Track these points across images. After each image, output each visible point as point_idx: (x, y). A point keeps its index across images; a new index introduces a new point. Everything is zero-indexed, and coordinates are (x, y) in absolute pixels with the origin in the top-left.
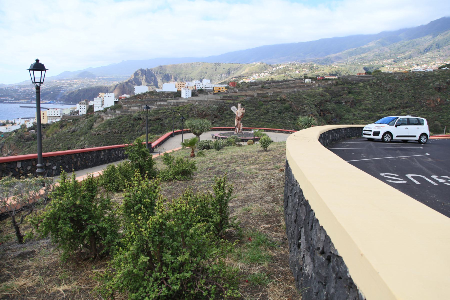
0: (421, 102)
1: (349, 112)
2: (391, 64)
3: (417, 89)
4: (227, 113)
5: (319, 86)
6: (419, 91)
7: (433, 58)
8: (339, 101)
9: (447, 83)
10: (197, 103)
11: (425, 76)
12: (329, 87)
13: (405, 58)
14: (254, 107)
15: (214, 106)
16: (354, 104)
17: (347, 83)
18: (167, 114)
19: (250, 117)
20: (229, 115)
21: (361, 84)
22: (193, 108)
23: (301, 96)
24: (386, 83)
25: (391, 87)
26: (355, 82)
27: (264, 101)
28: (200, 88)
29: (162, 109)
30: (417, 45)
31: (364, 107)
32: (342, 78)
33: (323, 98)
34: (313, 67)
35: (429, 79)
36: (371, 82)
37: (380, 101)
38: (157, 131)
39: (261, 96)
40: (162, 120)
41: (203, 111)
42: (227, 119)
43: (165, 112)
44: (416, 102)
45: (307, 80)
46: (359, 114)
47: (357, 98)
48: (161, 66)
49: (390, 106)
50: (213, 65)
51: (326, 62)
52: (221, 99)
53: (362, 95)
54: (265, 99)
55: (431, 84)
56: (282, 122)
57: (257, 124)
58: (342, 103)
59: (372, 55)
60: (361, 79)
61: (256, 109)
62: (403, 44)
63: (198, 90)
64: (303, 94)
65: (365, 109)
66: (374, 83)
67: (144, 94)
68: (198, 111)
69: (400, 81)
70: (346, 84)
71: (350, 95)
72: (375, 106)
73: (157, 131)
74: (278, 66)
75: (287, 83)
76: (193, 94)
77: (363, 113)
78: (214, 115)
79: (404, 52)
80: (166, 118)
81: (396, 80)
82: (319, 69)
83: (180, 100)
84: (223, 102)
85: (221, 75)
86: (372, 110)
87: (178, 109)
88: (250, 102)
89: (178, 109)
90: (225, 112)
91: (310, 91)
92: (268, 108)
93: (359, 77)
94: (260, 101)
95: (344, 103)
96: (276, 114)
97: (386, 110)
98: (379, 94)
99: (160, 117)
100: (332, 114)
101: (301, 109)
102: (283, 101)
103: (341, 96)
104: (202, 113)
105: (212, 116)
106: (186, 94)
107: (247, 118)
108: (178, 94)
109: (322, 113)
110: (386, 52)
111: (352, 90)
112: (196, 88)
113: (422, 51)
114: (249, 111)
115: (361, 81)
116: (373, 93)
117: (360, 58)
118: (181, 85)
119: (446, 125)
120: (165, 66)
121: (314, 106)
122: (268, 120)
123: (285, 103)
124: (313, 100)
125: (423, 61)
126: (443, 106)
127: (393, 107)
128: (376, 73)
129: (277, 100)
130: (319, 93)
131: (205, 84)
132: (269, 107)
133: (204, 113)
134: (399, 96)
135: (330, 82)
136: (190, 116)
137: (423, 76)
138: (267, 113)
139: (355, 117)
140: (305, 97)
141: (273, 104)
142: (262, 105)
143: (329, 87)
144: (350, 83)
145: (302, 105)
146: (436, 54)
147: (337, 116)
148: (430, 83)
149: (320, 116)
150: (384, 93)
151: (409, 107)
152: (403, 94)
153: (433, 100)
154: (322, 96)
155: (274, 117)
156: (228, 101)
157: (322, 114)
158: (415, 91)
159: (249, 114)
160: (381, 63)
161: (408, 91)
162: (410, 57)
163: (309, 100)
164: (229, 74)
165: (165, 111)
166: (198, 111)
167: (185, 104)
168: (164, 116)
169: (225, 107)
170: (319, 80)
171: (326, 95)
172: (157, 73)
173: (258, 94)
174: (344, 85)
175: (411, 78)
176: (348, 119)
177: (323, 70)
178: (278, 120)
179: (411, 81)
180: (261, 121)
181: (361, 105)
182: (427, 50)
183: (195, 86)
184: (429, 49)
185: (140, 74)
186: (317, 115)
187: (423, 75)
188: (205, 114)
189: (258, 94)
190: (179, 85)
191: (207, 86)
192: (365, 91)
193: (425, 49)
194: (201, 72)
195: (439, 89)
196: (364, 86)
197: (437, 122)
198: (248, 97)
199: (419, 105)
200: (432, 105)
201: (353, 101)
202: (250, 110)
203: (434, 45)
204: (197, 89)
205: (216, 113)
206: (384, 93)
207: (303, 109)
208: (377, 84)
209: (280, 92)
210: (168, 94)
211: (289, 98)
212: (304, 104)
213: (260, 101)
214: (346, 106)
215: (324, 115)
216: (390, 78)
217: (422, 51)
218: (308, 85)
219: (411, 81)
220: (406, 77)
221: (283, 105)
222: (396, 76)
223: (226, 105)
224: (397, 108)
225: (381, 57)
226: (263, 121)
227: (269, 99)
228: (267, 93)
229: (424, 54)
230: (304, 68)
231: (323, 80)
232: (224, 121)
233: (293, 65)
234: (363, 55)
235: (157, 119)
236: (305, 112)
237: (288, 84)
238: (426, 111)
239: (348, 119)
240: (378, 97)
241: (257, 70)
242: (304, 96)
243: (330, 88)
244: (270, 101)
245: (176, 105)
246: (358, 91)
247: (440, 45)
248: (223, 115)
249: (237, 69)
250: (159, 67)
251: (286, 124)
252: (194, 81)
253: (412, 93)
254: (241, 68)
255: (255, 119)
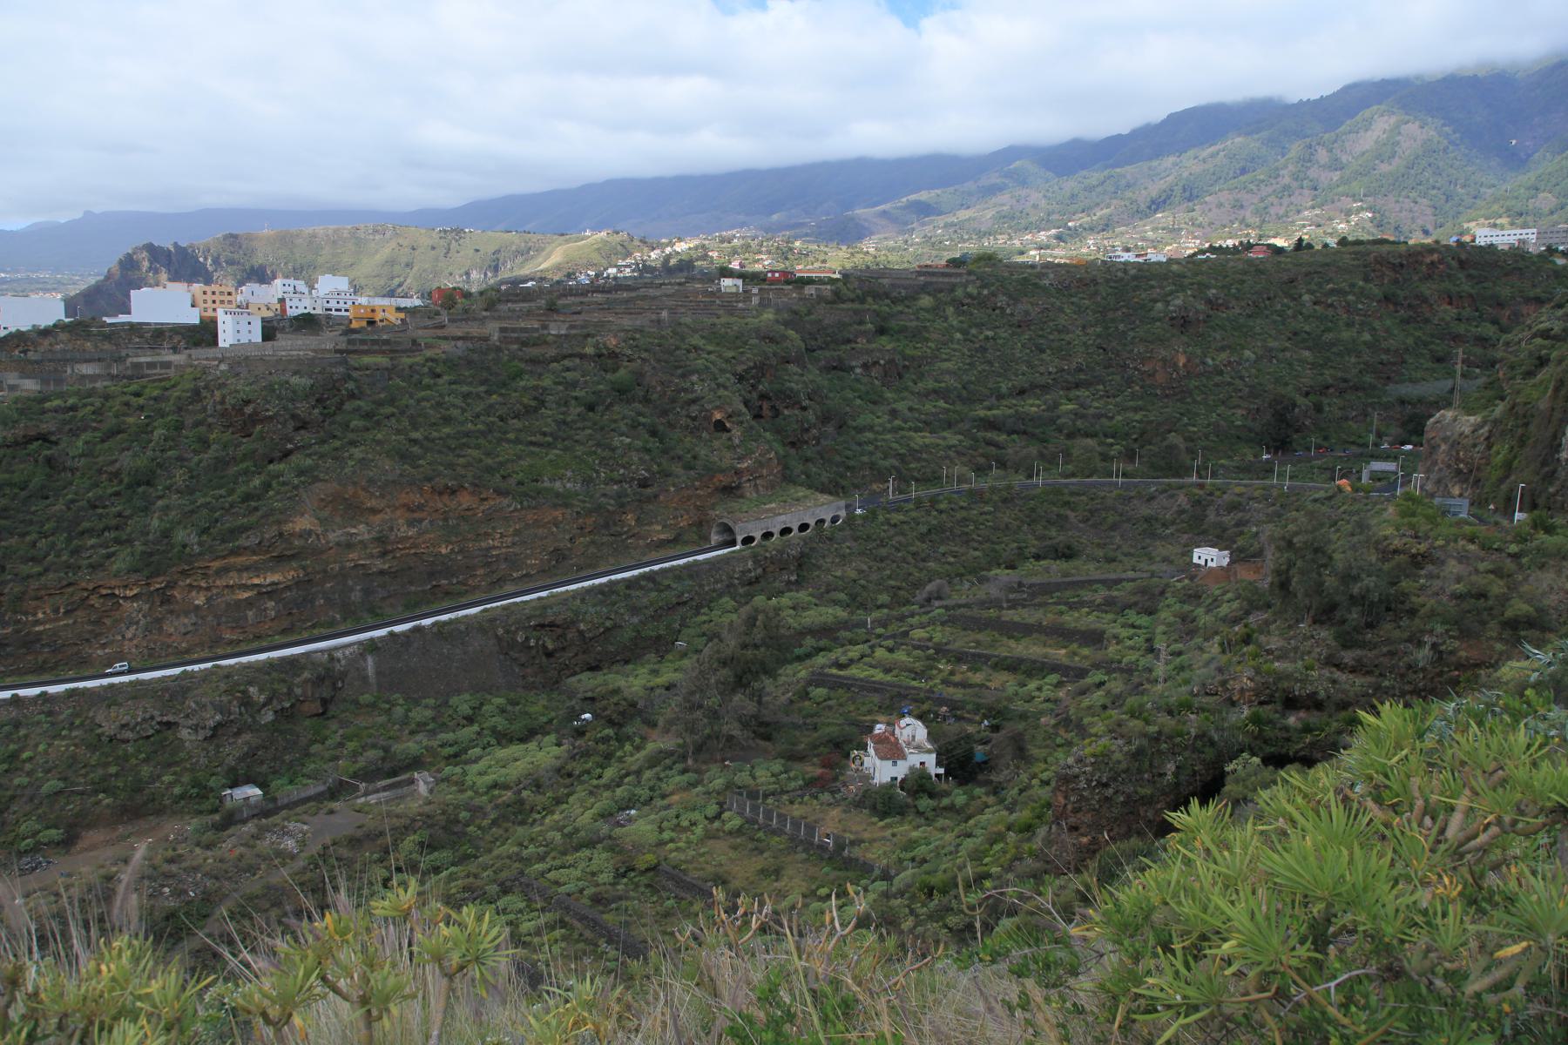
0: (1125, 366)
1: (875, 403)
2: (1047, 247)
3: (1113, 320)
4: (358, 409)
5: (764, 304)
6: (1121, 327)
7: (1174, 231)
8: (840, 359)
9: (1209, 302)
10: (223, 367)
11: (1146, 275)
12: (804, 310)
13: (1092, 229)
14: (483, 382)
15: (295, 380)
16: (895, 372)
17: (874, 298)
18: (80, 414)
19: (462, 423)
20: (368, 416)
21: (926, 301)
22: (206, 387)
23: (683, 339)
24: (1010, 297)
25: (1027, 313)
26: (903, 293)
27: (533, 361)
28: (301, 311)
29: (61, 395)
30: (1128, 186)
31: (930, 384)
32: (859, 279)
33: (770, 349)
34: (791, 249)
35: (1152, 287)
36: (959, 293)
37: (990, 363)
38: (24, 494)
39: (517, 340)
40: (56, 443)
41: (247, 402)
42: (351, 436)
43: (73, 408)
44: (1110, 366)
45: (727, 283)
46: (911, 409)
47: (908, 352)
48: (232, 236)
49: (1020, 381)
50: (434, 235)
51: (848, 233)
52: (337, 351)
53: (927, 340)
54: (534, 352)
55: (1159, 305)
56: (598, 445)
57: (488, 454)
58: (852, 368)
59: (989, 214)
60: (926, 284)
61: (489, 393)
62: (1087, 182)
63: (296, 318)
64: (695, 331)
65: (935, 391)
66: (970, 296)
67: (46, 332)
68: (222, 402)
69: (1058, 291)
70: (870, 300)
71: (884, 339)
72: (970, 382)
73: (24, 494)
74: (671, 244)
75: (652, 292)
76: (269, 332)
77: (929, 407)
78: (294, 417)
79: (1090, 208)
80: (74, 433)
81: (1044, 289)
82: (811, 258)
83: (201, 354)
84: (345, 362)
85: (468, 274)
86: (959, 397)
87: (137, 395)
88: (470, 363)
89: (137, 395)
90: (348, 406)
91: (723, 320)
92: (545, 389)
93: (919, 273)
94: (513, 357)
95: (858, 371)
96: (575, 410)
97: (1010, 395)
98: (987, 338)
99: (44, 428)
100: (804, 409)
101: (679, 392)
102: (607, 359)
103: (849, 341)
104: (240, 411)
105: (284, 424)
106: (235, 332)
107: (447, 430)
108: (205, 333)
109: (766, 405)
110: (1035, 206)
111: (893, 324)
112: (284, 311)
113: (1143, 206)
114: (458, 402)
115: (924, 289)
116: (965, 332)
117: (953, 225)
118: (217, 298)
119: (1204, 448)
120: (250, 238)
121: (733, 379)
122: (539, 438)
123: (615, 370)
124: (730, 354)
125: (1143, 239)
126: (1194, 383)
127: (1034, 386)
128: (982, 263)
129: (582, 356)
130: (757, 330)
131: (329, 292)
132: (547, 382)
133: (248, 410)
134: (1056, 344)
135: (810, 290)
136: (189, 421)
137: (1135, 278)
138: (536, 410)
139: (897, 422)
140: (701, 343)
141: (568, 369)
142: (519, 375)
143: (804, 310)
144: (887, 295)
145: (683, 376)
146: (1182, 216)
147: (825, 419)
148: (1155, 301)
149: (758, 417)
150: (1003, 333)
151: (1086, 384)
152: (1067, 338)
153: (1164, 360)
154: (772, 340)
155: (564, 422)
156: (367, 360)
157: (766, 412)
158: (1107, 328)
159: (455, 412)
160: (1017, 242)
161: (1084, 327)
162: (1106, 226)
163: (712, 357)
164: (496, 269)
165: (71, 401)
166: (222, 402)
167: (172, 372)
168: (65, 422)
169: (351, 385)
170: (774, 282)
171: (785, 337)
172: (216, 261)
173: (503, 330)
174: (863, 301)
175: (1094, 281)
176: (871, 428)
177: (824, 261)
178: (581, 436)
179: (1096, 293)
180: (509, 441)
181: (921, 376)
182: (1156, 205)
183: (282, 301)
184: (1164, 202)
185: (146, 264)
186: (740, 414)
187: (1133, 272)
188: (255, 413)
189: (503, 330)
190: (209, 297)
191: (333, 304)
192: (939, 324)
193: (1153, 202)
194: (391, 262)
195: (1183, 323)
196: (936, 310)
197: (1174, 438)
198: (460, 343)
199: (1118, 378)
200: (1160, 378)
201: (892, 361)
202: (466, 396)
203: (1178, 191)
204: (291, 313)
205: (302, 408)
206: (1003, 333)
207: (685, 390)
208: (982, 302)
209: (601, 325)
210: (159, 335)
211: (631, 347)
212: (692, 372)
213: (513, 357)
214: (865, 380)
215: (777, 413)
216: (1029, 281)
217: (1143, 206)
218: (729, 303)
219: (1096, 293)
220: (1080, 280)
221: (609, 376)
222: (1044, 275)
223: (355, 374)
224: (1045, 388)
225: (1013, 221)
226: (517, 441)
227: (552, 352)
228: (545, 327)
229: (1147, 216)
230: (760, 253)
231: (788, 283)
232: (337, 443)
233: (722, 242)
234: (963, 214)
235: (29, 440)
236: (694, 401)
237: (654, 298)
238: (1142, 398)
239: (871, 428)
240: (983, 350)
241: (596, 258)
242: (696, 340)
243: (809, 313)
244: (555, 360)
245: (130, 378)
246: (914, 324)
247: (1195, 192)
248: (338, 418)
249: (524, 253)
250: (226, 237)
251: (613, 450)
252: (278, 282)
253: (1099, 336)
254: (539, 250)
255: (483, 434)
